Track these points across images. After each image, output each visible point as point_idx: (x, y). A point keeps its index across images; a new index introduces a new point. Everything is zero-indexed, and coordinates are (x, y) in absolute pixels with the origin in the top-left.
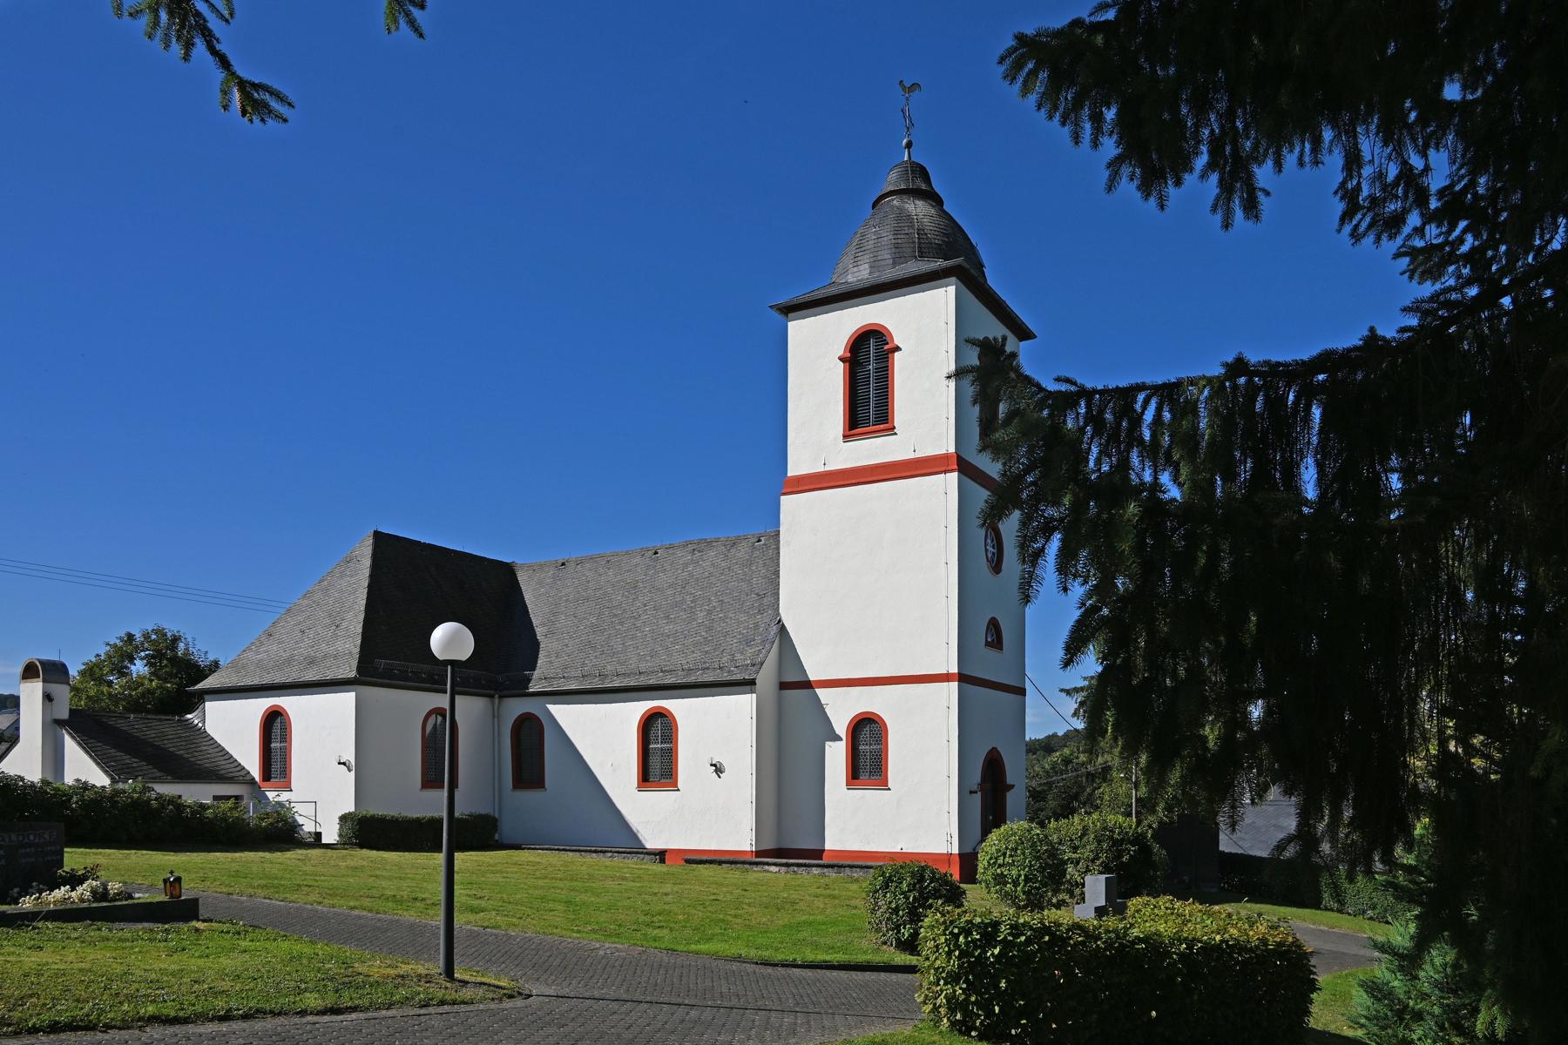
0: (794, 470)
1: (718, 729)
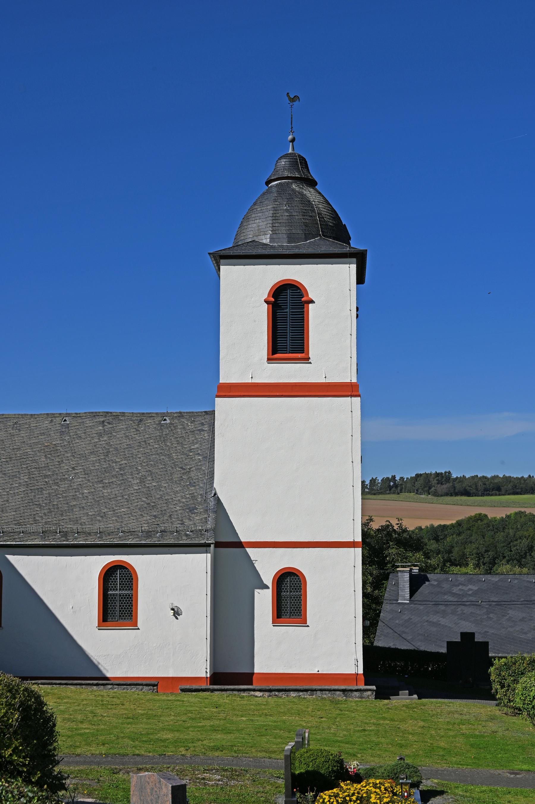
1: (178, 583)
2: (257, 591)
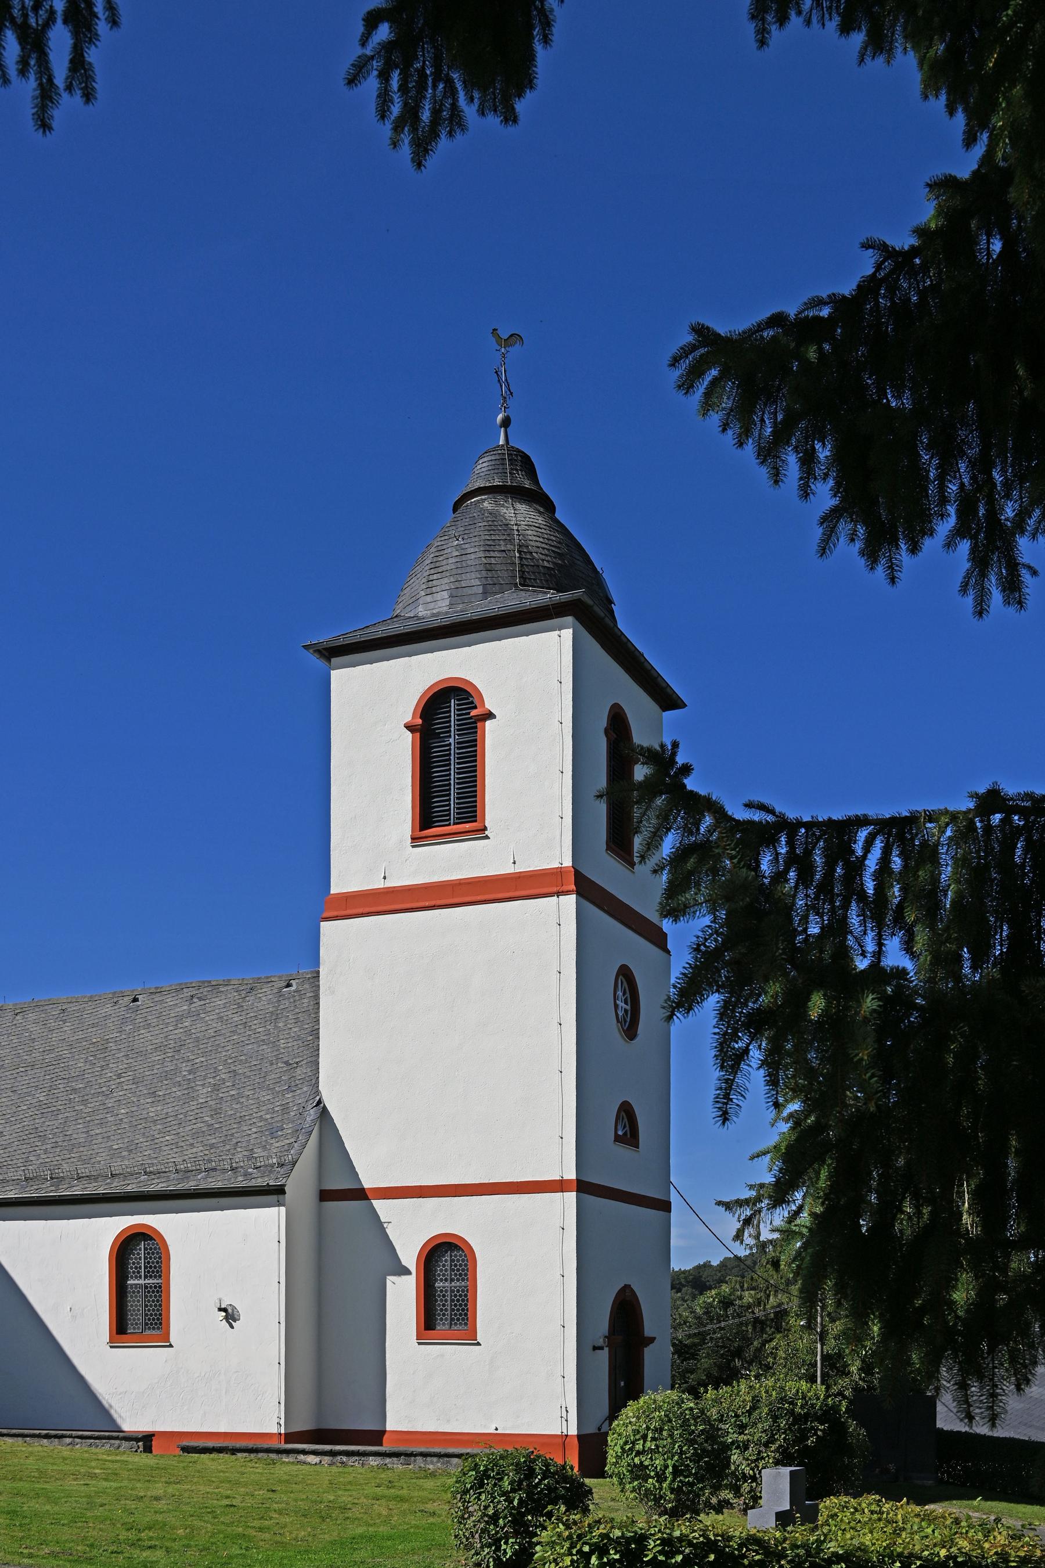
0: (337, 887)
1: (231, 1262)
2: (390, 1279)
